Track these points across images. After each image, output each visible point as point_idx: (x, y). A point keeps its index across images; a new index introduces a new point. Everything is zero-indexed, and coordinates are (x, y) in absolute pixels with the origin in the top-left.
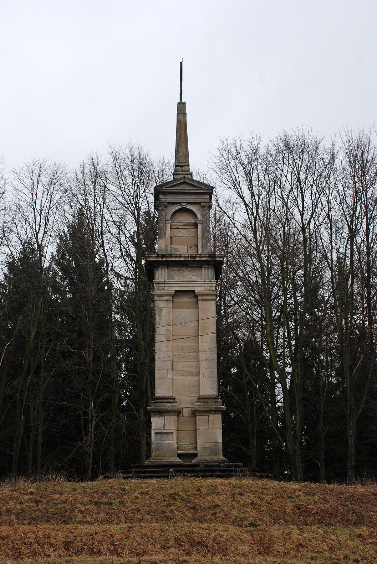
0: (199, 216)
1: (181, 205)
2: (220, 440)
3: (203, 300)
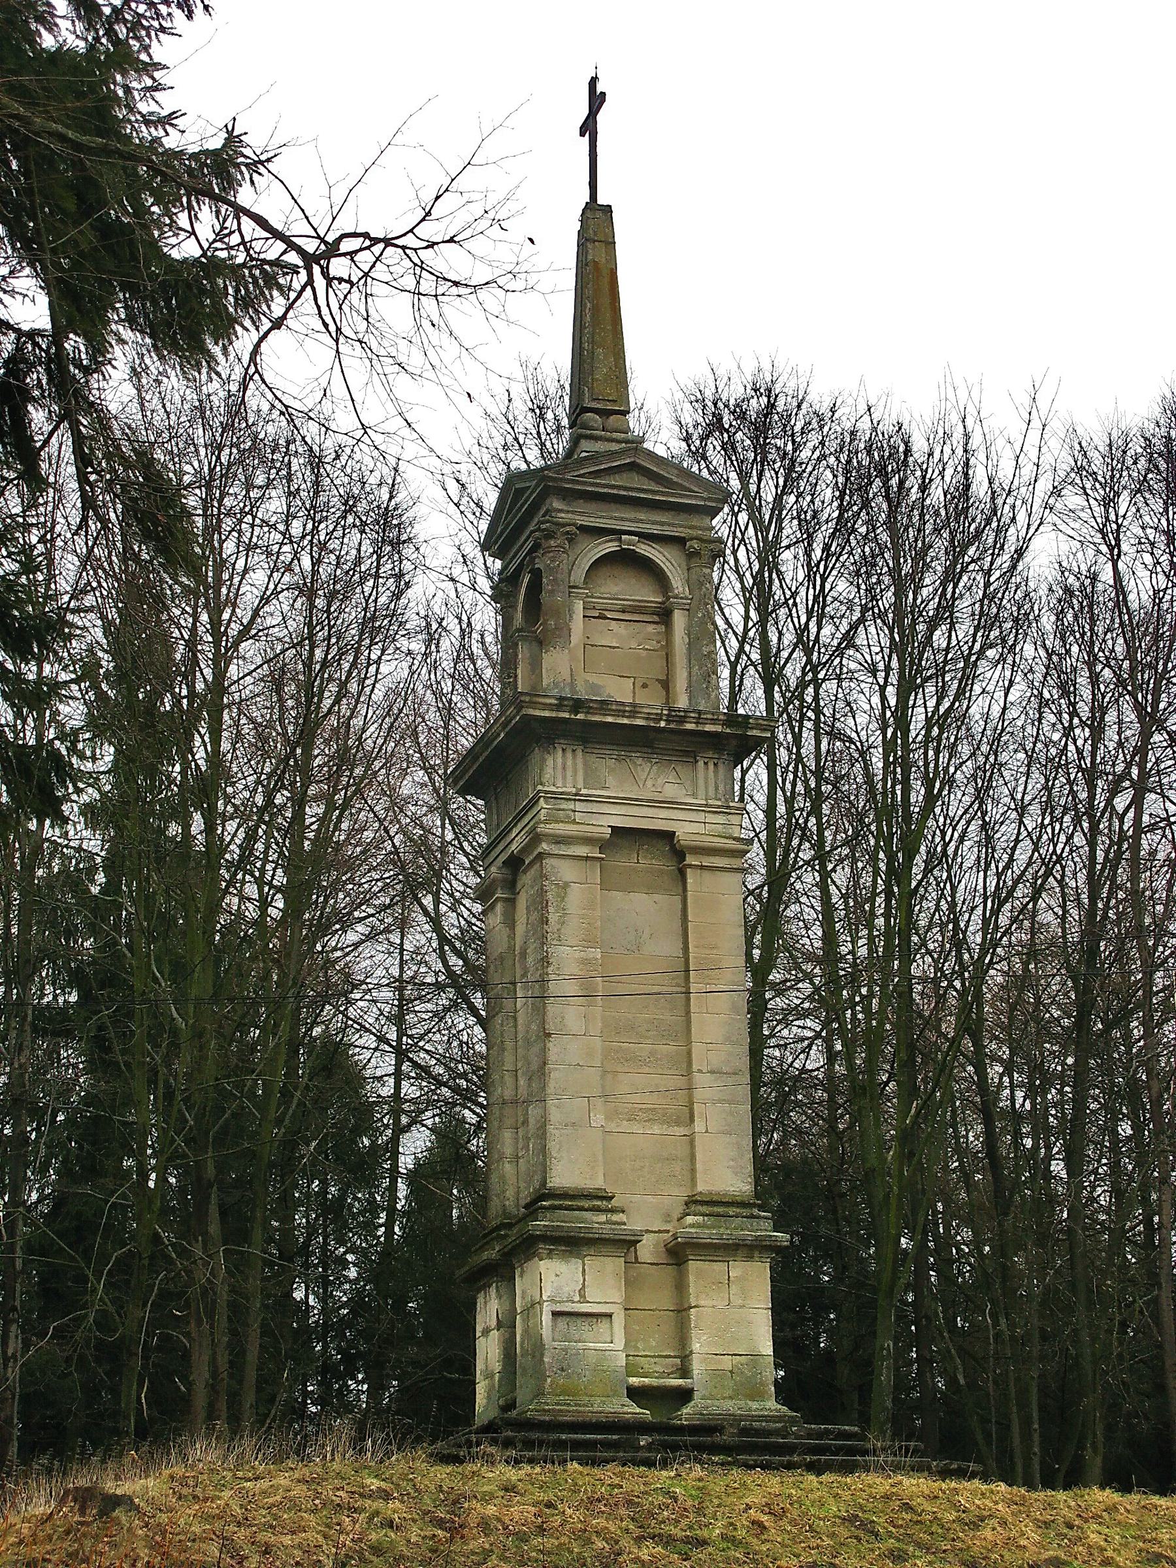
0: (678, 584)
1: (620, 540)
2: (767, 1348)
3: (702, 867)
